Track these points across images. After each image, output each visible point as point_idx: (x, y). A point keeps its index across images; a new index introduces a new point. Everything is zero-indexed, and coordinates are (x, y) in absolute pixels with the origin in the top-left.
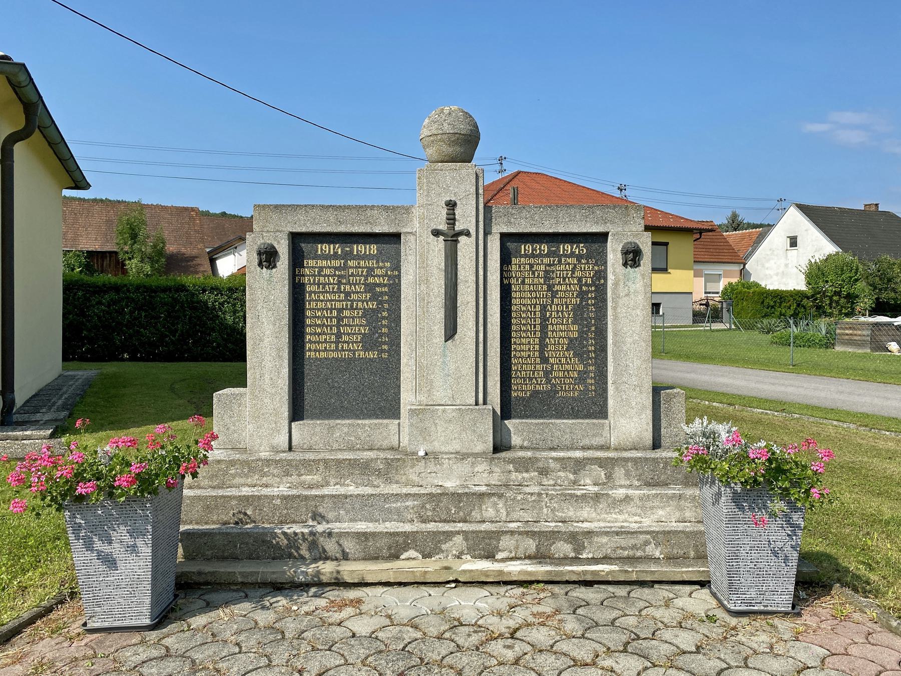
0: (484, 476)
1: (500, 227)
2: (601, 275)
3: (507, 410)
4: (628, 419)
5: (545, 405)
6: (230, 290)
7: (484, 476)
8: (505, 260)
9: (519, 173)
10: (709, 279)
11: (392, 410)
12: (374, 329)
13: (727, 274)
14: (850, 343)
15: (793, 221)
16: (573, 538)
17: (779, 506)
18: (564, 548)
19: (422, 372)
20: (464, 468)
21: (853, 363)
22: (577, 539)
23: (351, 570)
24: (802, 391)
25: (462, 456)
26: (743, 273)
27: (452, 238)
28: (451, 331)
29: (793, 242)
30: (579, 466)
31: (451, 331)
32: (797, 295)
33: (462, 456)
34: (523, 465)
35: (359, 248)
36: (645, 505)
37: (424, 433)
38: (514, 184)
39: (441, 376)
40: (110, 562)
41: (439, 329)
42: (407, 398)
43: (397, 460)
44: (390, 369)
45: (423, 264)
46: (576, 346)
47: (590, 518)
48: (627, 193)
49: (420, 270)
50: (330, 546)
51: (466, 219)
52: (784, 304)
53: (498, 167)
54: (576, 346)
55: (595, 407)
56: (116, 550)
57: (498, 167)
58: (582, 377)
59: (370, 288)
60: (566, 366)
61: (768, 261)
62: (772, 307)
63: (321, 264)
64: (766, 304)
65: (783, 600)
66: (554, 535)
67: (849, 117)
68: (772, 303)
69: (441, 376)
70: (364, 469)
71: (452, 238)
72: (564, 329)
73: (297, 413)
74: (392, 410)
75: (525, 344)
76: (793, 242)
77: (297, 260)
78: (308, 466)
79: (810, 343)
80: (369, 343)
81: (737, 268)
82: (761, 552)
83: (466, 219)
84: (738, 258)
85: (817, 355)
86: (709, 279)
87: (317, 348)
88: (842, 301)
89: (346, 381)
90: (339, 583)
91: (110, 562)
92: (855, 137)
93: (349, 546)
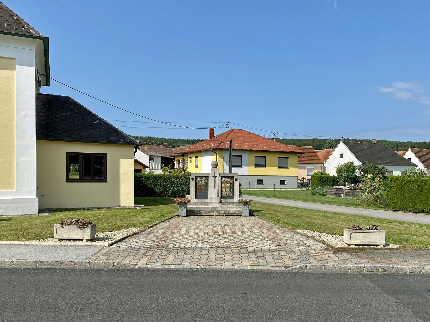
0: (218, 205)
1: (220, 176)
2: (233, 181)
3: (222, 198)
4: (236, 199)
5: (226, 197)
6: (149, 177)
7: (218, 205)
8: (221, 179)
9: (233, 129)
10: (309, 170)
11: (207, 198)
12: (205, 188)
13: (316, 168)
14: (331, 194)
15: (342, 147)
16: (228, 211)
17: (247, 206)
18: (227, 212)
19: (211, 193)
20: (216, 204)
21: (331, 200)
22: (229, 211)
23: (204, 214)
24: (298, 205)
25: (216, 203)
26: (323, 168)
27: (215, 177)
28: (215, 188)
29: (342, 156)
30: (229, 204)
31: (215, 188)
32: (334, 177)
33: (216, 203)
34: (223, 204)
35: (203, 178)
36: (237, 208)
37: (212, 200)
38: (230, 137)
39: (213, 194)
40: (182, 210)
41: (213, 188)
42: (209, 196)
43: (208, 204)
44: (207, 193)
45: (211, 180)
46: (230, 190)
47: (230, 209)
48: (277, 135)
49: (211, 181)
50: (201, 212)
51: (217, 175)
52: (329, 181)
53: (226, 126)
54: (230, 190)
55: (232, 197)
56: (183, 209)
57: (226, 126)
58: (231, 194)
59: (205, 183)
60: (229, 193)
61: (332, 163)
62: (324, 182)
63: (199, 180)
64: (321, 181)
65: (248, 215)
66: (226, 211)
67: (402, 85)
68: (324, 181)
69: (213, 194)
70: (205, 204)
71: (215, 177)
72: (228, 188)
73: (196, 198)
74: (207, 198)
75: (224, 190)
76: (342, 156)
77: (196, 180)
78: (198, 204)
79: (320, 194)
80: (204, 190)
81: (320, 166)
82: (246, 210)
83: (217, 175)
84: (321, 162)
85: (322, 197)
86: (309, 170)
87: (199, 190)
88: (348, 180)
89: (202, 195)
90: (203, 215)
91: (182, 210)
92: (405, 95)
93: (203, 212)
